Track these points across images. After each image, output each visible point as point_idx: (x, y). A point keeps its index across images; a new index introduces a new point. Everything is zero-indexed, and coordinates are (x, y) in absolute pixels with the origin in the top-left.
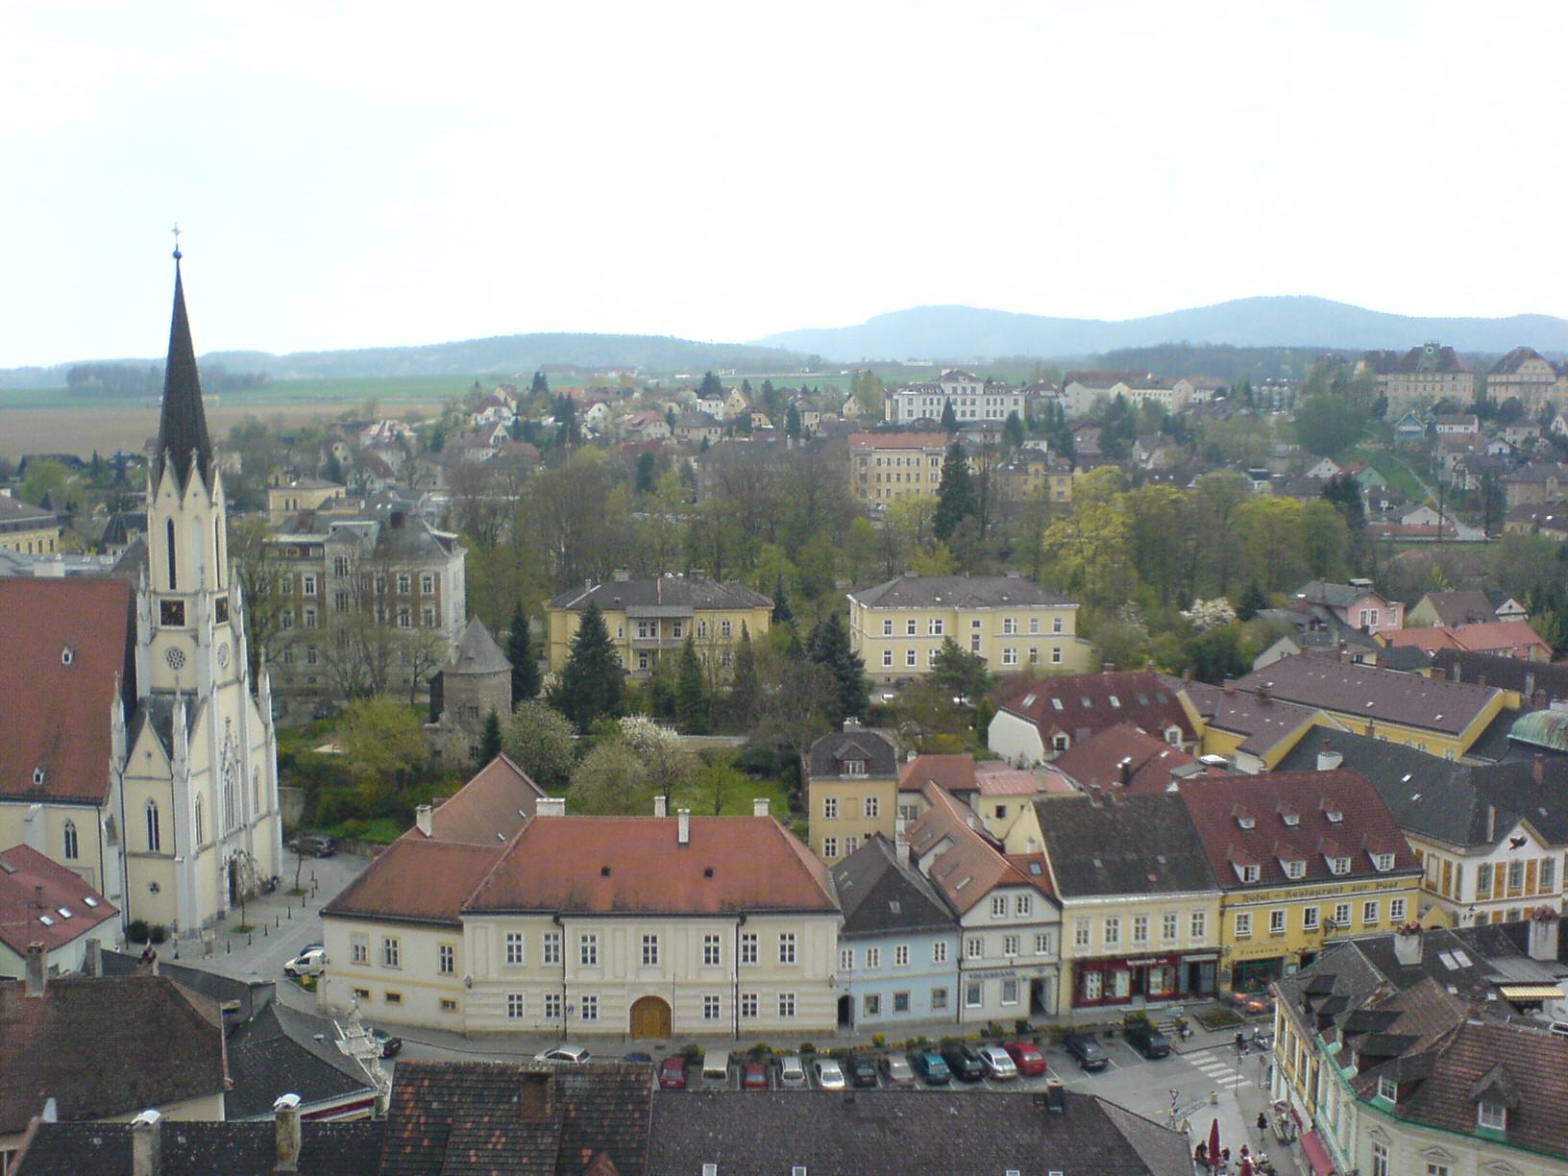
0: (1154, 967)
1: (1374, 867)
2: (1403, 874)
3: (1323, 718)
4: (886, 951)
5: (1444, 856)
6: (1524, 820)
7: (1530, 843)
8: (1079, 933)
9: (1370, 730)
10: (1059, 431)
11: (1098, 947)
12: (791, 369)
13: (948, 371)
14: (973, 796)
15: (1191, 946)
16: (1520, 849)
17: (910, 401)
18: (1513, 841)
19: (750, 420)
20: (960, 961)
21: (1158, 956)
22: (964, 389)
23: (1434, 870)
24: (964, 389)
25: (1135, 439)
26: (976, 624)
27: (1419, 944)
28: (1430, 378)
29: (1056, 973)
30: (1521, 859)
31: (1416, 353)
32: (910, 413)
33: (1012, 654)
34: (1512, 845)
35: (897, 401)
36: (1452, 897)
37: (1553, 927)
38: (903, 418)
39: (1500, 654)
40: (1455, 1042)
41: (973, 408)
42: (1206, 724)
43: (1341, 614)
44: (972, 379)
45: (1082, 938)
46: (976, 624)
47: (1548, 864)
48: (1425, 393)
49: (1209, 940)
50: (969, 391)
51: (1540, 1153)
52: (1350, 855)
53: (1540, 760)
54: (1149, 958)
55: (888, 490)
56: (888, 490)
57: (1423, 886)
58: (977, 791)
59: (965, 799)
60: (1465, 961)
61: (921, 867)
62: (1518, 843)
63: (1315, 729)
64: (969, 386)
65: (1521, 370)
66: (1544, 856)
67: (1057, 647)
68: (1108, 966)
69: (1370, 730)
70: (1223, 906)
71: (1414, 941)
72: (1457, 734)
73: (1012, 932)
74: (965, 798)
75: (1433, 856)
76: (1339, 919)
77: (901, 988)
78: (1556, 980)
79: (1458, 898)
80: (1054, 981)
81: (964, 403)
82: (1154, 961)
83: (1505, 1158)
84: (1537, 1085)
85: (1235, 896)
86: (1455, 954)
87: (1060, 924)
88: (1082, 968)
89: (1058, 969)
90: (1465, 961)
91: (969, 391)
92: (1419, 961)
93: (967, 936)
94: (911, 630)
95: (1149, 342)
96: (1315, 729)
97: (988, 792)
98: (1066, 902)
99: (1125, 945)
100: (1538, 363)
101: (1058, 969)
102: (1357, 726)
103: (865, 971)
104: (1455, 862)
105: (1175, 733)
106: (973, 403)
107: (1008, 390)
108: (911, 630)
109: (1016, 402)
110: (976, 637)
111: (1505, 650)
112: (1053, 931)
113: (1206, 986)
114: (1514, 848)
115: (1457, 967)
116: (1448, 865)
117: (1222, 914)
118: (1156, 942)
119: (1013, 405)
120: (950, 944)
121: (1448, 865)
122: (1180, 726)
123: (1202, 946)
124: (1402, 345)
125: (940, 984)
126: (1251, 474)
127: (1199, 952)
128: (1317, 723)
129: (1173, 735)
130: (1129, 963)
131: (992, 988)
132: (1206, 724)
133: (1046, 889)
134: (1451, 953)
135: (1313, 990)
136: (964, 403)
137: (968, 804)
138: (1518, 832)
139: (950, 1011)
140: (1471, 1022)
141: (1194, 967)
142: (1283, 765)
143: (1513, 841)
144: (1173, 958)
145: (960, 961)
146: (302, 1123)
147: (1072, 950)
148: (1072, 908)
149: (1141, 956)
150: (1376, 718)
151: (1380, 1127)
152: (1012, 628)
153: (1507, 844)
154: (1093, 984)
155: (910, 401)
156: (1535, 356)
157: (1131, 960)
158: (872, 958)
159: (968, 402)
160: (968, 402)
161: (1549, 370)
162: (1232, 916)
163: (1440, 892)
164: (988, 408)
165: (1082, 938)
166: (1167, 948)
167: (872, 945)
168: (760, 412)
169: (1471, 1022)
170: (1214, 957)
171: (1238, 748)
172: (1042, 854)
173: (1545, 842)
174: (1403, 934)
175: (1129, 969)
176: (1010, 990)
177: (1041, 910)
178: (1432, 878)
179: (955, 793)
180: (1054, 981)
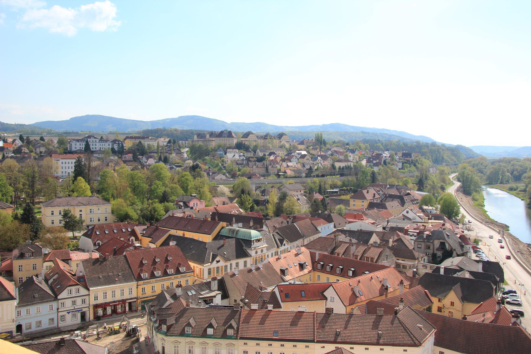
0: (118, 304)
3: (173, 232)
4: (33, 309)
7: (221, 261)
8: (95, 297)
10: (120, 152)
11: (101, 301)
12: (131, 134)
13: (88, 135)
14: (69, 261)
15: (129, 297)
17: (76, 145)
18: (216, 261)
19: (22, 150)
20: (58, 309)
21: (119, 301)
22: (93, 141)
23: (197, 271)
24: (93, 141)
25: (143, 156)
26: (81, 211)
28: (226, 139)
29: (88, 309)
30: (219, 266)
31: (222, 132)
32: (76, 148)
33: (92, 219)
35: (71, 144)
36: (202, 278)
37: (216, 282)
38: (74, 149)
39: (229, 213)
41: (96, 146)
42: (142, 236)
43: (187, 204)
44: (95, 138)
45: (96, 298)
46: (81, 211)
47: (226, 266)
48: (225, 143)
49: (134, 295)
50: (94, 141)
54: (116, 302)
55: (66, 172)
56: (66, 172)
58: (71, 259)
59: (67, 262)
60: (194, 293)
61: (49, 283)
62: (218, 262)
64: (94, 140)
65: (249, 137)
66: (225, 265)
67: (106, 217)
68: (104, 306)
69: (184, 234)
70: (138, 285)
71: (180, 289)
73: (74, 299)
74: (67, 262)
76: (171, 286)
77: (39, 319)
79: (203, 278)
80: (88, 312)
81: (93, 145)
82: (118, 303)
84: (445, 338)
85: (141, 282)
87: (89, 295)
88: (96, 307)
89: (89, 308)
90: (194, 293)
91: (94, 141)
93: (60, 301)
94: (52, 214)
95: (297, 130)
96: (170, 236)
97: (74, 259)
98: (90, 289)
99: (109, 299)
100: (253, 136)
101: (89, 308)
103: (26, 316)
105: (133, 239)
106: (96, 145)
107: (106, 141)
108: (52, 214)
109: (109, 145)
110: (81, 215)
112: (87, 297)
113: (134, 308)
115: (191, 294)
117: (137, 288)
118: (118, 297)
119: (107, 146)
120: (55, 304)
121: (201, 269)
122: (134, 237)
123: (132, 297)
124: (218, 130)
125: (51, 317)
126: (175, 165)
127: (131, 299)
129: (132, 240)
130: (111, 304)
131: (69, 317)
132: (142, 236)
133: (75, 284)
135: (152, 305)
136: (93, 145)
137: (68, 264)
139: (55, 325)
141: (130, 304)
142: (162, 245)
143: (216, 261)
144: (124, 301)
145: (58, 309)
147: (93, 302)
148: (92, 290)
149: (114, 302)
151: (163, 338)
152: (92, 212)
153: (215, 262)
154: (100, 312)
155: (76, 145)
156: (252, 133)
157: (111, 303)
158: (28, 312)
159: (94, 145)
160: (94, 145)
161: (256, 137)
162: (140, 288)
164: (80, 146)
165: (96, 298)
166: (122, 299)
167: (28, 308)
168: (25, 147)
170: (135, 300)
171: (149, 242)
172: (84, 275)
175: (111, 306)
176: (74, 316)
177: (83, 291)
178: (197, 273)
179: (63, 260)
180: (88, 312)
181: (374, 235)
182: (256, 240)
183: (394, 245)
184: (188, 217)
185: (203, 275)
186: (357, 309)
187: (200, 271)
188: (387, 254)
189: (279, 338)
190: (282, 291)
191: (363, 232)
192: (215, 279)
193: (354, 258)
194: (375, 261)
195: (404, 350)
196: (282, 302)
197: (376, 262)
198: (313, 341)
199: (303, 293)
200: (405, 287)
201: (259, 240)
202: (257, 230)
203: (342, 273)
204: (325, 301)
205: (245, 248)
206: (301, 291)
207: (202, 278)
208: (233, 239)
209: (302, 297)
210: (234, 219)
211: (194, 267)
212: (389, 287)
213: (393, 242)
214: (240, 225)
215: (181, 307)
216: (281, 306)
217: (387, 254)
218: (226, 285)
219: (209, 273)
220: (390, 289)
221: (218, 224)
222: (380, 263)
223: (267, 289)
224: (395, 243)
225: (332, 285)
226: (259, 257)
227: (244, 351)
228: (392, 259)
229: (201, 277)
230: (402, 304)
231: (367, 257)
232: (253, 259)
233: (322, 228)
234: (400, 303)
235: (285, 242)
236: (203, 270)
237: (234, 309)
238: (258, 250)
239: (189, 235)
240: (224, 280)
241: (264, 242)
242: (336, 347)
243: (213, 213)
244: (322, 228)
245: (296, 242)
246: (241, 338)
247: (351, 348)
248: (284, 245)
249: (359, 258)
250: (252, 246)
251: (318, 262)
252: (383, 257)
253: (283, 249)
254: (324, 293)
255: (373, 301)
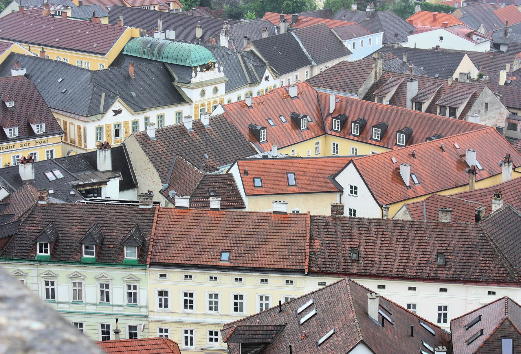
1: (33, 132)
2: (52, 135)
3: (18, 48)
5: (77, 123)
6: (119, 99)
9: (43, 52)
16: (119, 116)
18: (114, 111)
23: (72, 133)
27: (32, 168)
34: (114, 114)
36: (83, 147)
37: (108, 153)
40: (30, 214)
47: (135, 123)
51: (65, 263)
52: (16, 126)
53: (133, 64)
57: (69, 142)
62: (117, 112)
63: (12, 55)
69: (43, 52)
71: (29, 166)
72: (104, 54)
75: (72, 123)
78: (107, 180)
83: (133, 273)
86: (54, 172)
92: (34, 178)
102: (35, 51)
104: (82, 124)
111: (154, 5)
114: (115, 115)
115: (55, 179)
116: (79, 128)
121: (79, 128)
128: (14, 52)
134: (52, 172)
138: (117, 105)
140: (40, 202)
143: (114, 111)
146: (129, 332)
150: (31, 43)
153: (110, 113)
163: (77, 144)
169: (40, 202)
173: (133, 113)
174: (22, 163)
178: (73, 137)
181: (466, 58)
182: (201, 66)
183: (509, 82)
184: (56, 15)
185: (85, 141)
186: (405, 211)
187: (79, 132)
188: (486, 101)
189: (232, 265)
190: (246, 172)
191: (442, 53)
192: (106, 148)
193: (414, 108)
194: (459, 113)
195: (441, 290)
196: (247, 195)
197: (461, 117)
198: (301, 272)
199: (291, 177)
200: (516, 170)
201: (208, 67)
202: (206, 47)
203: (384, 140)
204: (338, 195)
205: (179, 85)
206: (287, 173)
207: (83, 147)
208: (152, 64)
209: (289, 185)
210: (160, 23)
211: (65, 123)
212: (480, 168)
213: (508, 75)
214: (172, 34)
215: (29, 202)
216: (244, 204)
217: (487, 100)
218: (129, 160)
219: (99, 136)
220: (482, 172)
221: (122, 30)
222: (471, 119)
223: (218, 170)
224: (514, 78)
225: (352, 161)
226: (209, 104)
227: (159, 292)
228: (499, 111)
229: (80, 143)
230: (497, 202)
231: (441, 107)
232: (196, 108)
233: (354, 44)
234: (494, 201)
235: (267, 73)
236: (85, 130)
237: (141, 207)
238: (205, 88)
239: (53, 54)
240: (126, 150)
241: (219, 71)
242: (320, 284)
243: (115, 7)
244: (354, 44)
245: (294, 74)
246: (154, 264)
247: (379, 287)
248: (267, 79)
249: (424, 107)
250: (193, 80)
251: (333, 116)
252: (476, 106)
253: (265, 88)
254: (337, 179)
255: (442, 196)
